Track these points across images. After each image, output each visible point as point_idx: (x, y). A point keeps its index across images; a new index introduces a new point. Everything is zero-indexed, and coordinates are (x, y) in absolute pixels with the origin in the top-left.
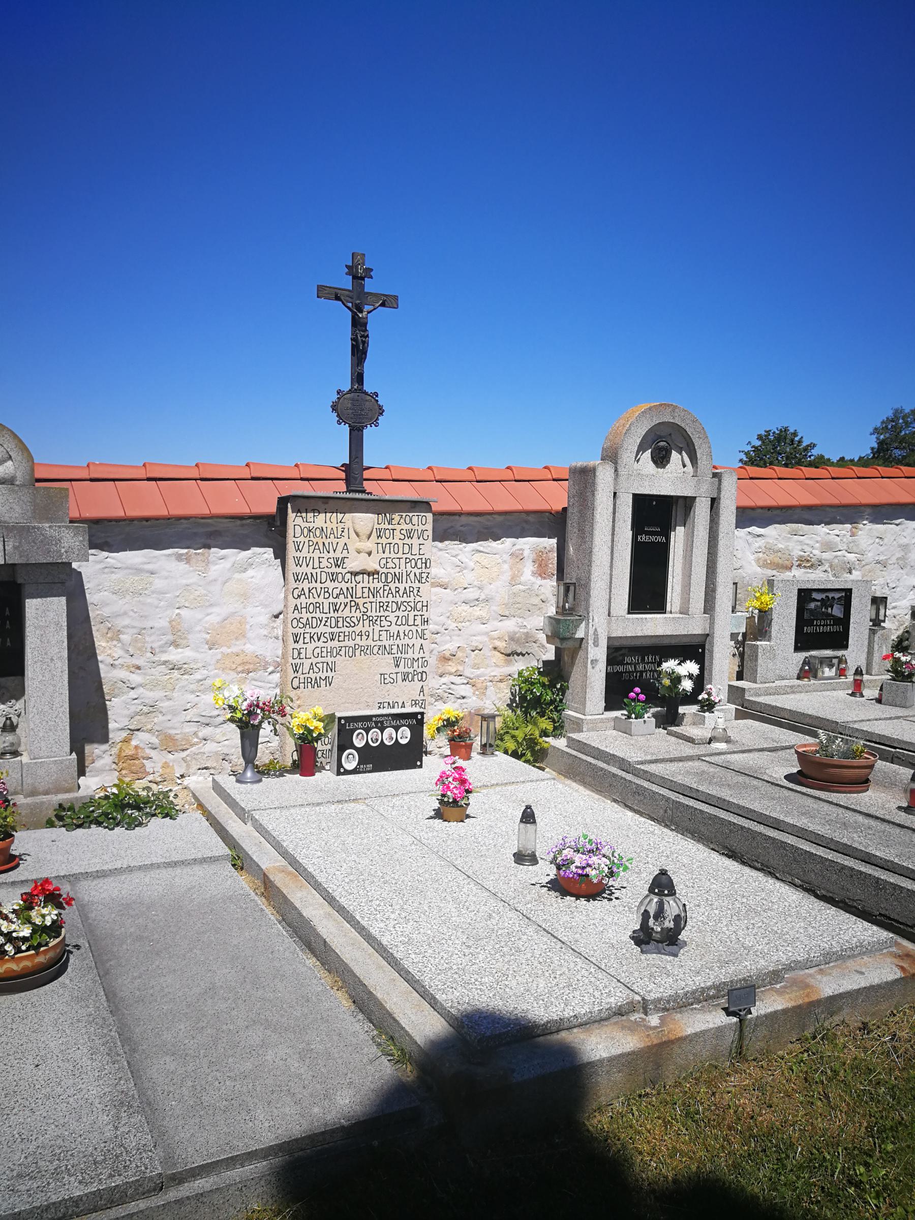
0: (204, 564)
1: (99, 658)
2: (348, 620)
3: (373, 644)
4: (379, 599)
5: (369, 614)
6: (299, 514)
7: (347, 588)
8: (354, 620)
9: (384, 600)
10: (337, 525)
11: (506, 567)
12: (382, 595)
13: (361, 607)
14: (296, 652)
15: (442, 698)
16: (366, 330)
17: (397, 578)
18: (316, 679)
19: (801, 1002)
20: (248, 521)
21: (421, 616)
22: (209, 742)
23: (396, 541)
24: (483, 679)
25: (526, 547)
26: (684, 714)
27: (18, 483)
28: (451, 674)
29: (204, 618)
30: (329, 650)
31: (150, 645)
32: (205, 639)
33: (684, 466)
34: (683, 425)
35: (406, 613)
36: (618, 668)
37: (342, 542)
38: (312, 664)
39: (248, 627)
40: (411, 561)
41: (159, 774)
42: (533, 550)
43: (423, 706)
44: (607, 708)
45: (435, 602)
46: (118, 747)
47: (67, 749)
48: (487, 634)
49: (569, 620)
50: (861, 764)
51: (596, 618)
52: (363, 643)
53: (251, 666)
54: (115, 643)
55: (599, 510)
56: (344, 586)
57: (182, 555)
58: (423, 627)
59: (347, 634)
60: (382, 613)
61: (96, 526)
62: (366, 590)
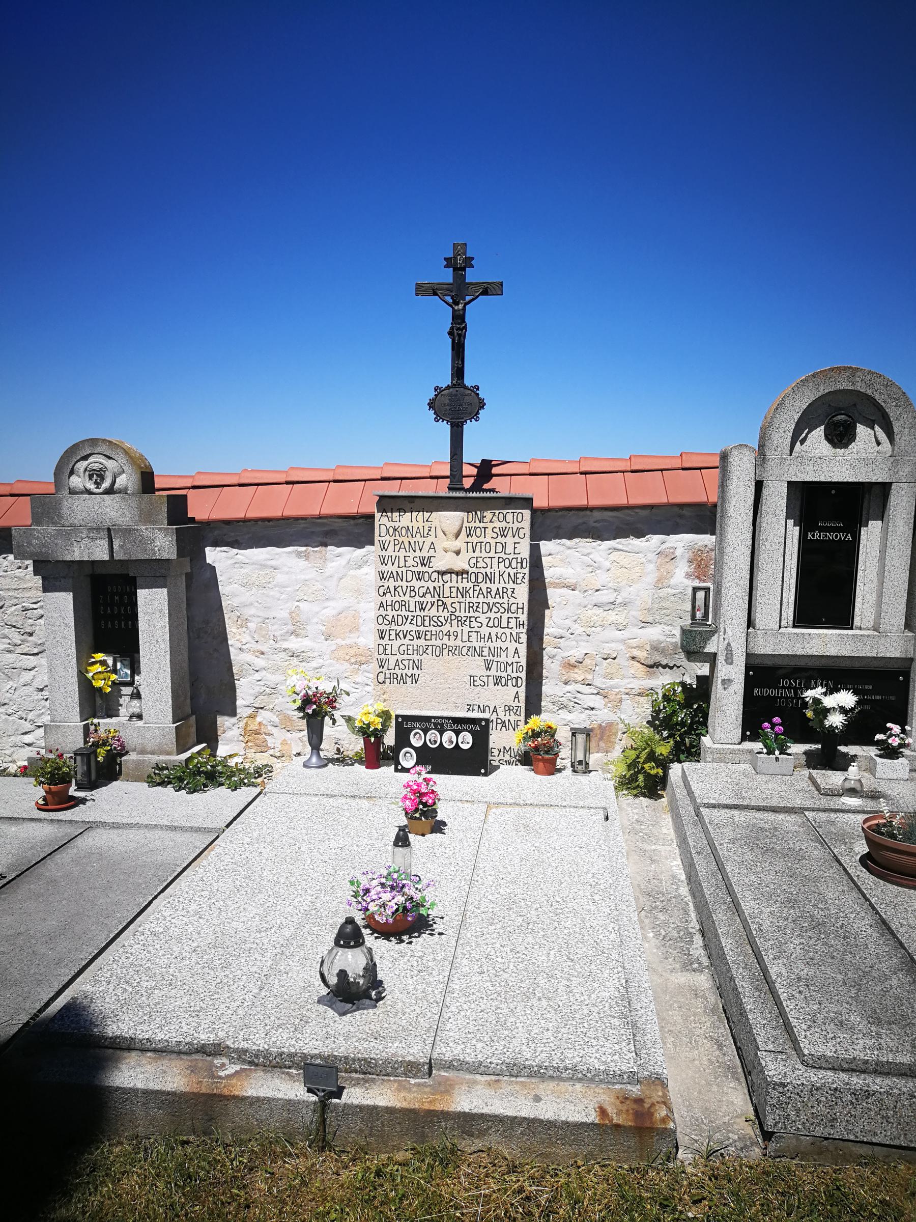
1: (230, 642)
2: (435, 619)
3: (462, 645)
4: (468, 600)
5: (457, 614)
6: (384, 514)
7: (434, 587)
8: (441, 619)
9: (474, 600)
11: (651, 567)
12: (471, 595)
13: (449, 607)
14: (381, 648)
15: (566, 707)
16: (464, 321)
17: (489, 578)
19: (417, 1106)
20: (361, 521)
21: (516, 618)
23: (488, 539)
24: (617, 690)
25: (680, 545)
26: (856, 756)
27: (129, 492)
28: (577, 682)
29: (320, 611)
30: (415, 648)
31: (273, 634)
33: (878, 444)
34: (869, 392)
35: (498, 615)
37: (428, 541)
40: (504, 560)
41: (278, 749)
42: (689, 548)
43: (518, 713)
44: (744, 738)
45: (560, 603)
46: (245, 721)
47: (170, 718)
48: (623, 641)
49: (695, 631)
50: (900, 848)
52: (452, 643)
54: (244, 629)
55: (733, 503)
56: (431, 585)
57: (301, 552)
58: (518, 631)
59: (434, 633)
60: (472, 614)
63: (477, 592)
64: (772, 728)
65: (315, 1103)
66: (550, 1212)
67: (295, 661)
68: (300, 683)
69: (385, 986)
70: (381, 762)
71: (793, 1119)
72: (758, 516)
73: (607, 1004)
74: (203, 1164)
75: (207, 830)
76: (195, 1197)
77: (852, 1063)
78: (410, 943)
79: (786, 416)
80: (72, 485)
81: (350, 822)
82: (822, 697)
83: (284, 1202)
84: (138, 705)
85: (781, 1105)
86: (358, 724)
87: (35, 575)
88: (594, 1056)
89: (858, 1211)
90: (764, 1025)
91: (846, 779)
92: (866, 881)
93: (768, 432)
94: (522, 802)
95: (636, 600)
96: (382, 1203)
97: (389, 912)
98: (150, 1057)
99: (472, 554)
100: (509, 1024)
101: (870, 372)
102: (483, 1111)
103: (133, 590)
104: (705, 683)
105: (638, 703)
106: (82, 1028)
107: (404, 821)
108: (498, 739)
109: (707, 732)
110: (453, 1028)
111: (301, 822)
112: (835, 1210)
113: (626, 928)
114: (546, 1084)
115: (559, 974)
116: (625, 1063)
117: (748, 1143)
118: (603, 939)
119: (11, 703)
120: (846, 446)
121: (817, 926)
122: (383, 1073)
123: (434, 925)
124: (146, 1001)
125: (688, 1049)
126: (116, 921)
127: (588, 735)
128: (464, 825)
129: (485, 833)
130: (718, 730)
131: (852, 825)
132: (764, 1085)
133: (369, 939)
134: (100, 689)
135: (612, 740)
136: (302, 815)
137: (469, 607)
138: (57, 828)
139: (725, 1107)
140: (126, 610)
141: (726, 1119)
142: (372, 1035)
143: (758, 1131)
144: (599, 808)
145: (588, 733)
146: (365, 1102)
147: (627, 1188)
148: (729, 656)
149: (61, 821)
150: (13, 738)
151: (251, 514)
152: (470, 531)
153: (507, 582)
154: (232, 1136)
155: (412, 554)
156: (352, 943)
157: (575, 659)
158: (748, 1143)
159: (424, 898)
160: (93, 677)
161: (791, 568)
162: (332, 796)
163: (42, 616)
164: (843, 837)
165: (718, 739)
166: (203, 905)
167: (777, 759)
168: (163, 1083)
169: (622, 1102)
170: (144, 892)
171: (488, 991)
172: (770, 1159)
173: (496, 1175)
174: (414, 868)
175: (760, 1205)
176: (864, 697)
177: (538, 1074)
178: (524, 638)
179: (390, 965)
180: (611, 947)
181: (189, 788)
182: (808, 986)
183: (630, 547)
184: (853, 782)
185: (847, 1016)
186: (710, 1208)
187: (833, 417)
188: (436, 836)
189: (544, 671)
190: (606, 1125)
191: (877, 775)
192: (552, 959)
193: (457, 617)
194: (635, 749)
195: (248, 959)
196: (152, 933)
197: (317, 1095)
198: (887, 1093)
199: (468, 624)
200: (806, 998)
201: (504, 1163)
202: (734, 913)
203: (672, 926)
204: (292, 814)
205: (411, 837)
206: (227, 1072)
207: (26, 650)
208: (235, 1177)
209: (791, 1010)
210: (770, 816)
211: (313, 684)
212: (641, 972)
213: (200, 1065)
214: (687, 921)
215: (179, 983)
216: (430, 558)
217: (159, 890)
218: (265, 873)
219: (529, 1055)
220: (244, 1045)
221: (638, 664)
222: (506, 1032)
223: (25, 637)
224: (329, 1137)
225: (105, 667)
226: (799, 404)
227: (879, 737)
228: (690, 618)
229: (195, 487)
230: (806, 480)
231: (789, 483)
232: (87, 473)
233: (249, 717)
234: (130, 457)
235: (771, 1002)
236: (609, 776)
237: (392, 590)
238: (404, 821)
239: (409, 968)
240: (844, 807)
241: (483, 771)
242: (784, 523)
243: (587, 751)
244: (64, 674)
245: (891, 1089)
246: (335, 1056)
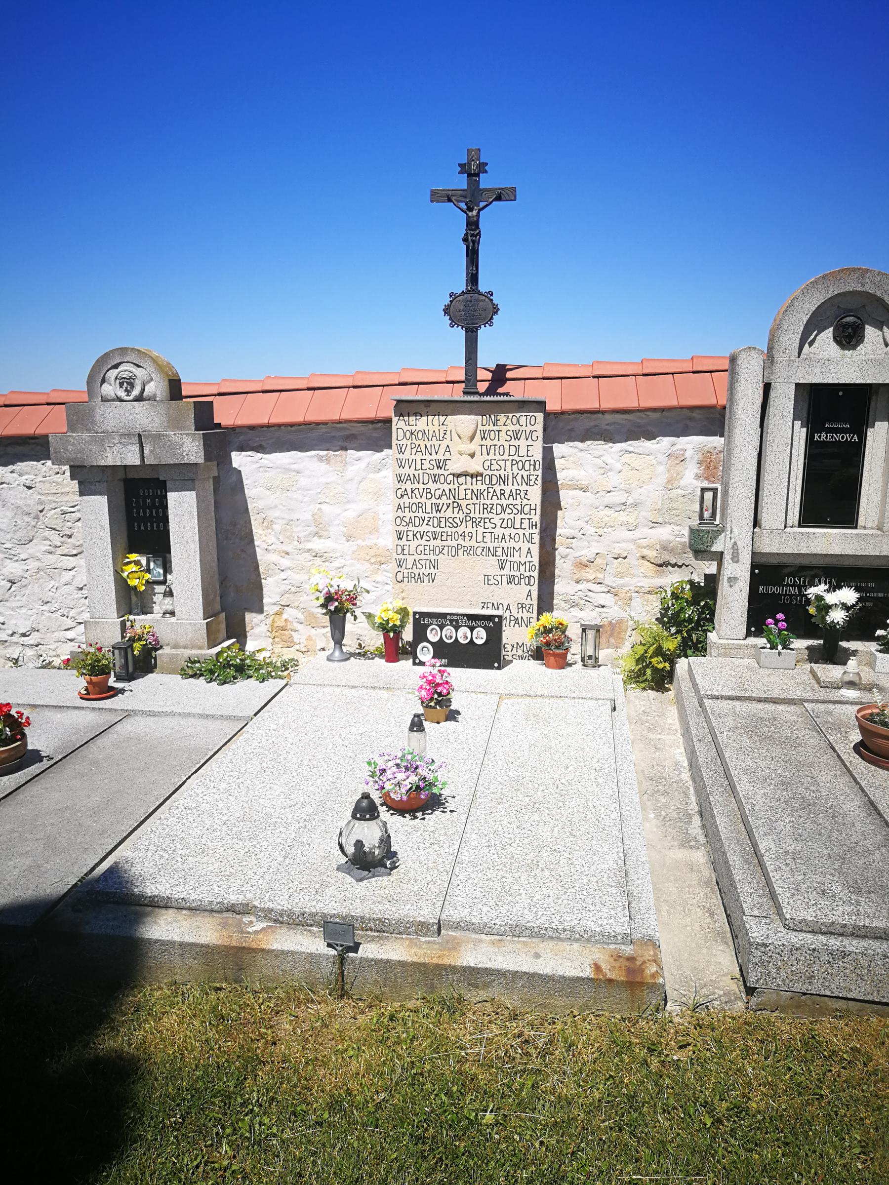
0: (342, 465)
1: (256, 543)
2: (450, 520)
3: (476, 545)
4: (483, 501)
5: (472, 515)
6: (401, 418)
7: (450, 490)
8: (457, 520)
9: (488, 502)
10: (439, 428)
11: (661, 469)
12: (486, 497)
13: (464, 509)
14: (399, 548)
15: (577, 605)
16: (478, 227)
17: (502, 480)
18: (419, 574)
19: (426, 960)
20: (379, 425)
21: (529, 519)
23: (502, 442)
24: (627, 589)
26: (856, 651)
27: (157, 399)
30: (432, 549)
32: (343, 532)
34: (878, 293)
35: (512, 516)
36: (774, 589)
37: (444, 444)
39: (380, 523)
40: (517, 463)
41: (303, 645)
42: (697, 450)
43: (530, 610)
44: (749, 634)
45: (572, 505)
46: (272, 618)
47: (201, 614)
49: (703, 531)
51: (735, 531)
52: (467, 543)
53: (383, 559)
54: (270, 531)
55: (741, 405)
56: (446, 487)
57: (322, 456)
58: (531, 531)
59: (449, 534)
60: (486, 515)
61: (251, 432)
62: (469, 492)
63: (491, 494)
64: (776, 624)
65: (334, 956)
66: (547, 1053)
67: (318, 561)
68: (322, 581)
69: (399, 857)
70: (400, 656)
71: (774, 976)
72: (766, 418)
73: (605, 875)
74: (234, 1007)
75: (236, 718)
76: (228, 1035)
77: (830, 926)
78: (423, 819)
79: (794, 318)
80: (104, 393)
81: (370, 711)
82: (824, 594)
83: (306, 1040)
84: (171, 602)
85: (762, 963)
86: (378, 621)
87: (71, 480)
88: (591, 919)
89: (830, 1056)
90: (751, 893)
91: (845, 673)
92: (858, 767)
93: (777, 335)
94: (532, 694)
95: (646, 501)
96: (395, 1043)
97: (404, 791)
98: (185, 915)
99: (486, 457)
100: (513, 891)
101: (879, 273)
102: (487, 966)
103: (164, 493)
104: (712, 581)
105: (647, 601)
106: (124, 888)
107: (420, 710)
108: (510, 635)
109: (714, 628)
110: (461, 894)
111: (324, 710)
112: (809, 1055)
113: (628, 808)
114: (545, 943)
115: (562, 849)
116: (620, 926)
117: (733, 998)
118: (605, 817)
119: (53, 601)
120: (854, 347)
121: (808, 806)
122: (396, 931)
123: (446, 804)
124: (181, 866)
125: (681, 916)
126: (153, 798)
127: (598, 631)
128: (477, 713)
129: (496, 721)
130: (724, 626)
131: (849, 716)
132: (747, 946)
133: (384, 813)
134: (135, 588)
135: (622, 636)
136: (325, 705)
137: (484, 509)
138: (99, 716)
139: (713, 967)
140: (157, 513)
141: (713, 977)
142: (386, 898)
143: (742, 988)
144: (606, 699)
145: (598, 629)
146: (379, 957)
147: (618, 1034)
148: (735, 555)
149: (102, 709)
150: (56, 634)
151: (275, 420)
152: (484, 434)
153: (520, 484)
154: (260, 984)
156: (368, 816)
158: (733, 998)
159: (436, 778)
160: (128, 576)
161: (797, 469)
162: (353, 687)
163: (80, 519)
164: (839, 727)
165: (723, 634)
166: (232, 784)
167: (780, 653)
168: (197, 936)
169: (615, 960)
170: (180, 772)
171: (494, 863)
172: (751, 1012)
173: (498, 1022)
174: (428, 752)
175: (740, 1050)
176: (866, 595)
177: (538, 934)
178: (536, 538)
179: (404, 839)
180: (612, 824)
181: (220, 680)
182: (794, 859)
183: (641, 449)
184: (851, 675)
185: (829, 886)
186: (694, 1052)
187: (842, 319)
188: (451, 724)
189: (556, 570)
190: (600, 980)
191: (877, 669)
192: (556, 835)
193: (471, 518)
194: (644, 645)
195: (273, 832)
196: (187, 809)
197: (336, 950)
198: (862, 953)
200: (792, 869)
201: (506, 1012)
202: (730, 795)
203: (673, 808)
204: (316, 704)
205: (426, 724)
206: (254, 929)
207: (66, 551)
208: (263, 1019)
209: (777, 880)
210: (771, 707)
211: (334, 584)
212: (639, 848)
213: (230, 922)
214: (687, 804)
215: (211, 852)
216: (445, 460)
217: (193, 771)
218: (290, 756)
219: (531, 917)
220: (270, 905)
222: (510, 898)
223: (65, 539)
224: (347, 987)
225: (139, 567)
226: (808, 306)
227: (880, 632)
228: (698, 518)
229: (220, 394)
230: (813, 382)
231: (797, 385)
232: (118, 381)
233: (276, 614)
234: (158, 365)
235: (759, 874)
236: (618, 670)
237: (409, 492)
238: (420, 710)
239: (422, 841)
240: (842, 699)
241: (496, 665)
242: (790, 424)
243: (596, 646)
244: (101, 573)
245: (866, 950)
246: (352, 916)
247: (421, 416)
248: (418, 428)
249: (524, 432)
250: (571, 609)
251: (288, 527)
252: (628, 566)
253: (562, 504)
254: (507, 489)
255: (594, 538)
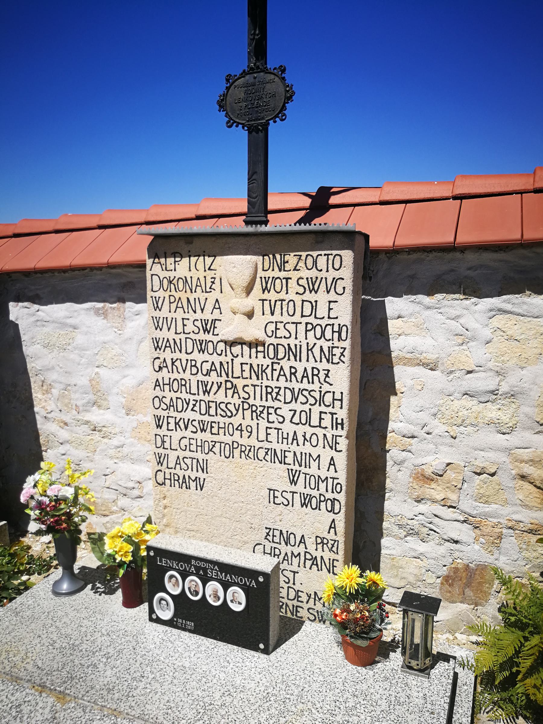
1: (36, 409)
2: (223, 406)
3: (258, 445)
4: (265, 383)
5: (251, 401)
6: (157, 260)
7: (221, 363)
8: (231, 407)
9: (273, 384)
12: (270, 377)
14: (159, 439)
15: (417, 534)
21: (332, 414)
22: (126, 513)
23: (291, 295)
24: (495, 521)
28: (434, 501)
35: (307, 407)
37: (212, 297)
38: (178, 457)
40: (314, 328)
43: (334, 549)
45: (412, 388)
48: (508, 451)
52: (244, 441)
56: (217, 360)
57: (99, 309)
59: (222, 425)
60: (270, 403)
62: (246, 368)
67: (97, 436)
95: (531, 390)
99: (269, 317)
105: (528, 544)
135: (485, 589)
137: (267, 393)
152: (267, 283)
153: (318, 359)
155: (192, 316)
157: (432, 469)
178: (343, 444)
183: (525, 307)
189: (388, 481)
193: (251, 406)
199: (265, 417)
221: (531, 487)
247: (182, 257)
248: (178, 274)
249: (324, 280)
250: (408, 538)
251: (66, 393)
252: (497, 487)
253: (397, 386)
254: (300, 367)
255: (444, 440)
